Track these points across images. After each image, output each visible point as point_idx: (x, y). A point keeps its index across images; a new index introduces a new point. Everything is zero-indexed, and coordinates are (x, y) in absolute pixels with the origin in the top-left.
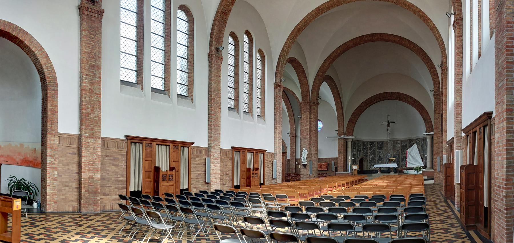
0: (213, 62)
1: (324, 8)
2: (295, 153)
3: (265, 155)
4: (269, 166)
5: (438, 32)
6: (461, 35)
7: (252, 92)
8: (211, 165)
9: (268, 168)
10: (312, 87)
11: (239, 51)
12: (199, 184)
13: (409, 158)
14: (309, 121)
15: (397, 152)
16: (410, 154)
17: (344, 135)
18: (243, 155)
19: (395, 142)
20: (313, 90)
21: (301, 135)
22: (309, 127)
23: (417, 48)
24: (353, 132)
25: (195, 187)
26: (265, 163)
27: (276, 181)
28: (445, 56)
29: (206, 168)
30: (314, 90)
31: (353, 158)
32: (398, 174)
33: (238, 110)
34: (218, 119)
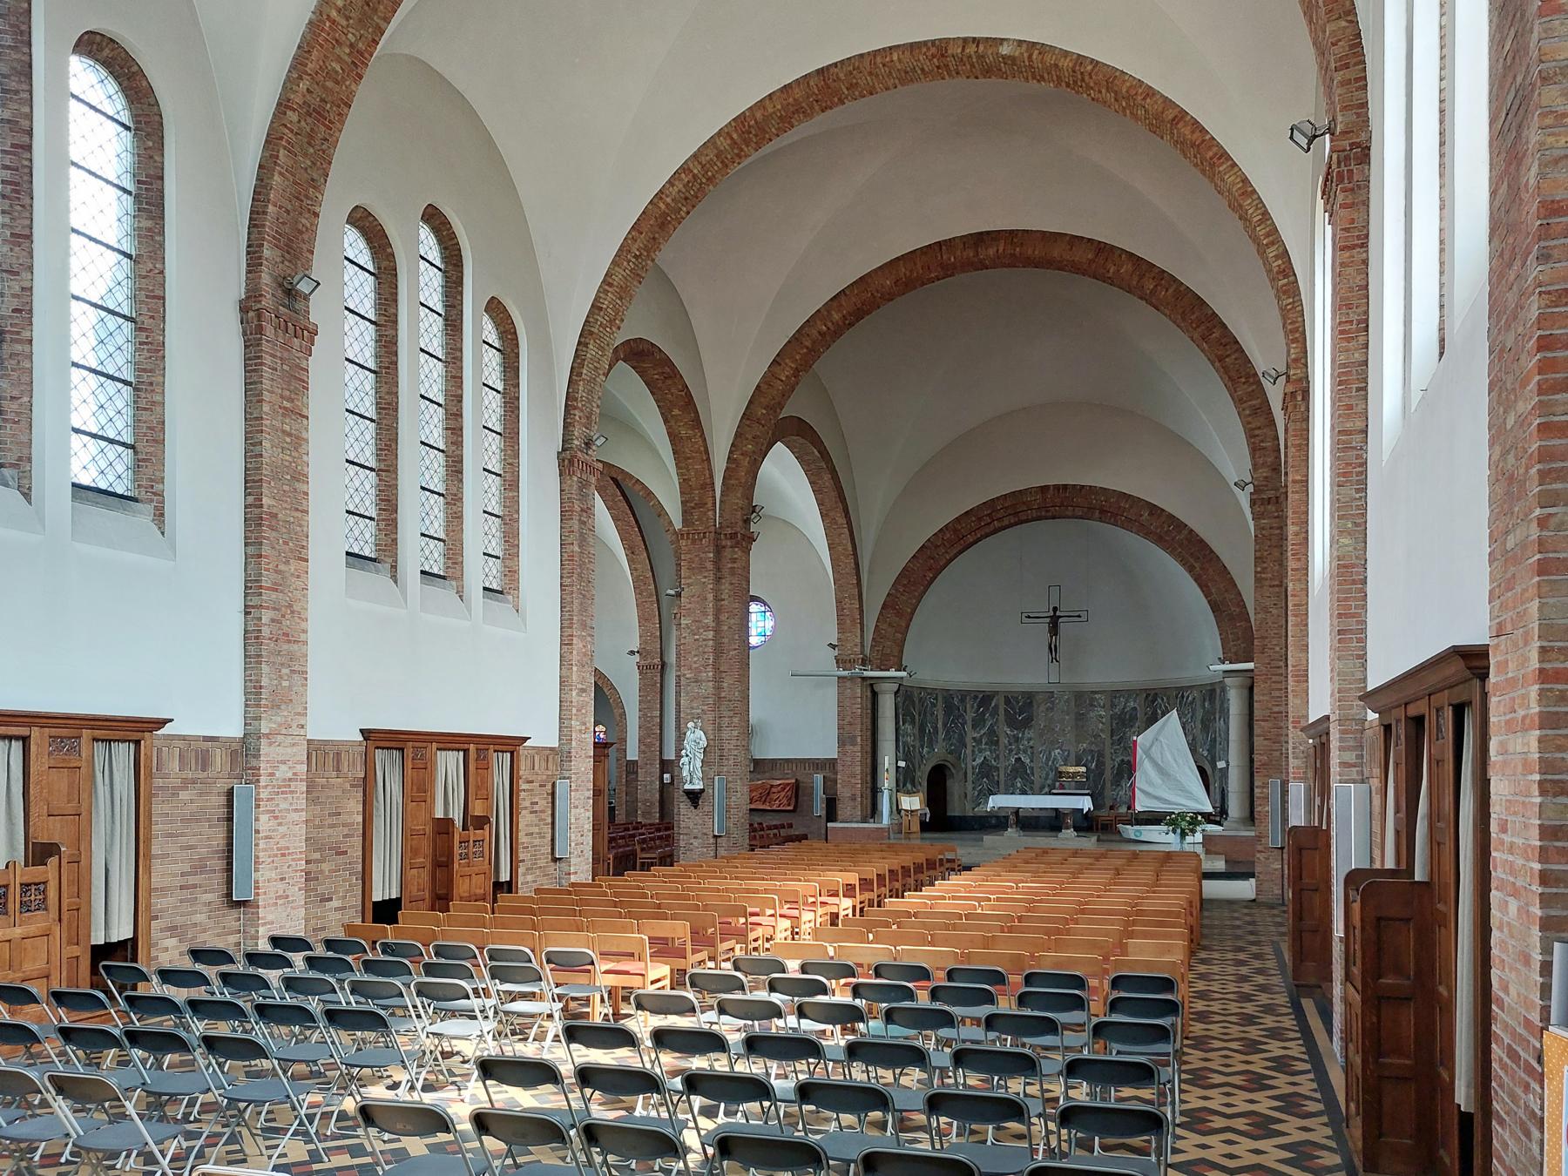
0: (265, 346)
1: (766, 118)
2: (661, 734)
3: (518, 760)
5: (1266, 213)
6: (1359, 237)
8: (257, 819)
9: (531, 813)
12: (195, 912)
14: (710, 611)
16: (1147, 753)
17: (863, 664)
18: (419, 764)
19: (1083, 699)
21: (679, 666)
22: (710, 637)
23: (1171, 291)
25: (172, 930)
26: (519, 791)
27: (566, 869)
28: (1296, 330)
29: (230, 831)
31: (902, 764)
32: (1094, 839)
33: (394, 567)
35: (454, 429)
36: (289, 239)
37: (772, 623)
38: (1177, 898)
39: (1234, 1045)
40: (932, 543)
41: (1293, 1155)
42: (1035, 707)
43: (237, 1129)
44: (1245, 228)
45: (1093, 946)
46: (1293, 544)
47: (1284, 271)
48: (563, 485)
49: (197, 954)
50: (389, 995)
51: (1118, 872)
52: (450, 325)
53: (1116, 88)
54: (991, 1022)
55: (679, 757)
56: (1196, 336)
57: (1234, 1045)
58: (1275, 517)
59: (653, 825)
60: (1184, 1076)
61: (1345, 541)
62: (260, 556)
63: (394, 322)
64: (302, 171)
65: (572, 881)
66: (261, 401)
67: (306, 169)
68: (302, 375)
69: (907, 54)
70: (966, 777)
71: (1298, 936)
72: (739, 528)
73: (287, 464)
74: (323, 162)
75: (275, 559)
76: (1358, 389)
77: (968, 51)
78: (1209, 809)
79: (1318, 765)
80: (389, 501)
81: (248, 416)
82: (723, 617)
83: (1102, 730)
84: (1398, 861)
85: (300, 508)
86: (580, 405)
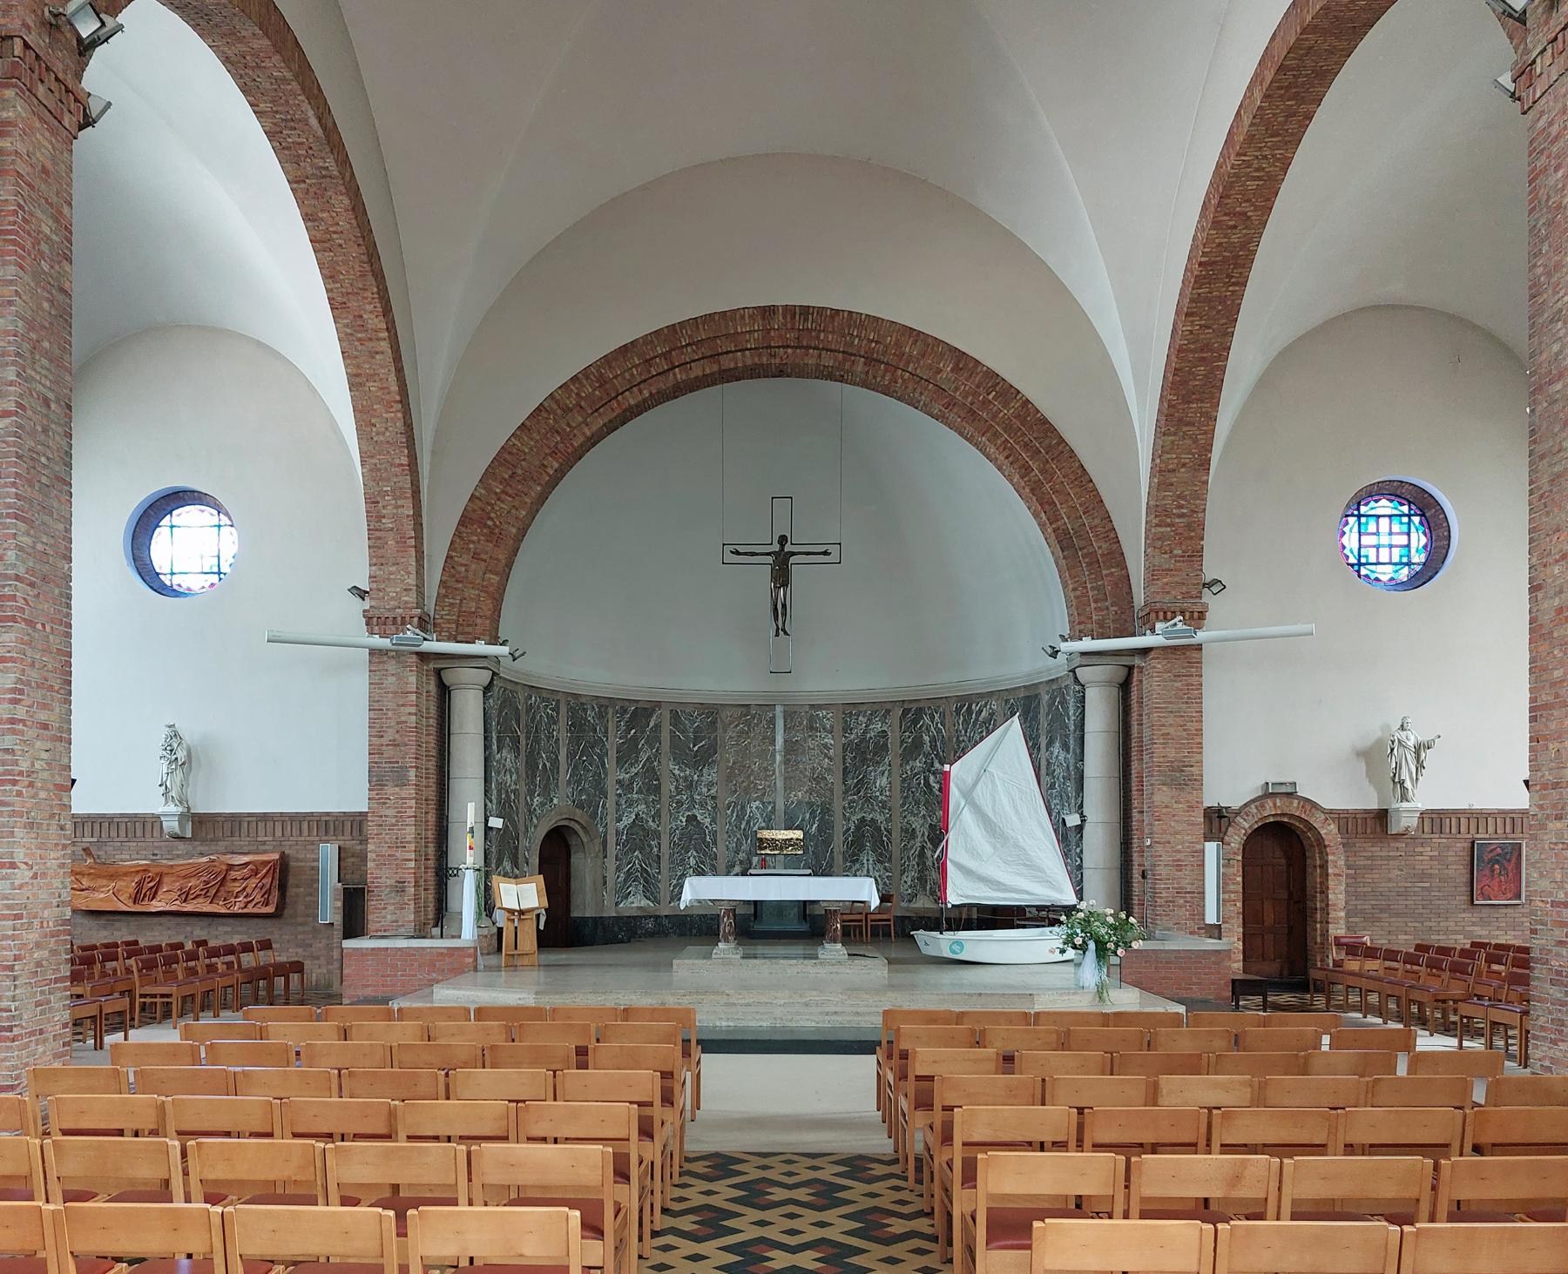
15: (810, 791)
16: (968, 795)
19: (804, 718)
24: (497, 611)
31: (497, 823)
40: (557, 402)
42: (720, 731)
50: (1444, 556)
83: (829, 770)
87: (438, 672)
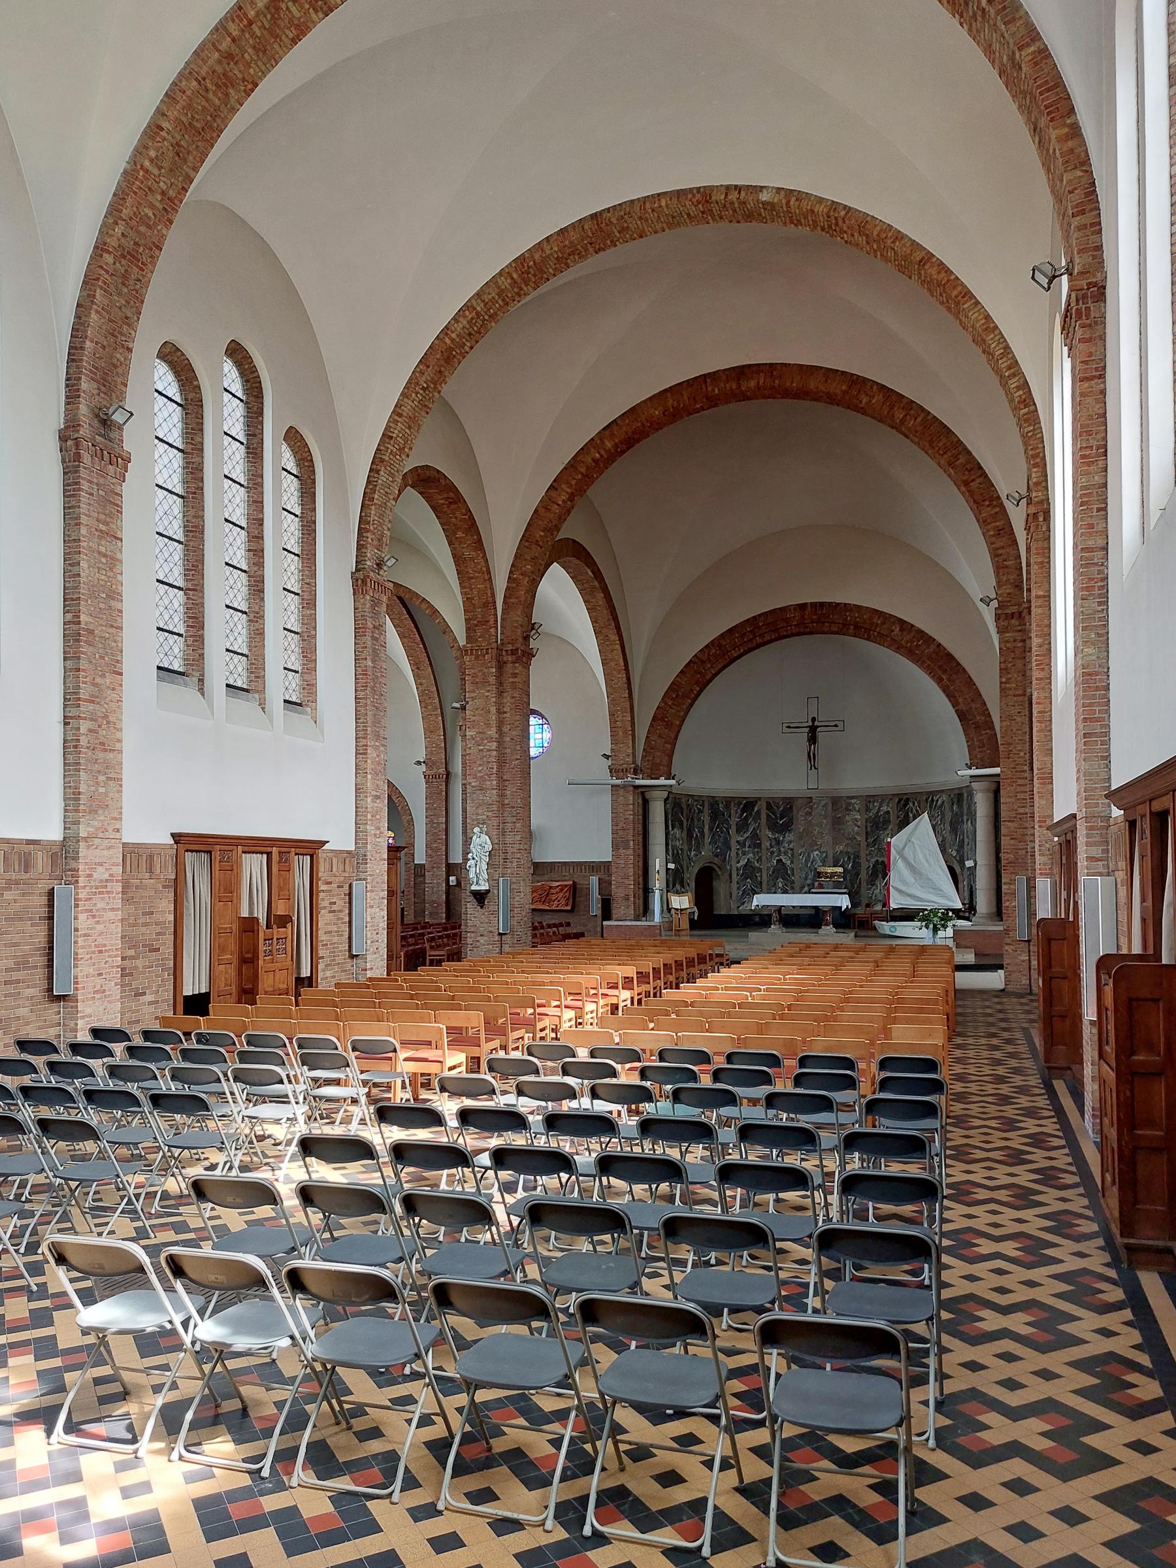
0: (83, 473)
1: (544, 259)
2: (447, 839)
3: (318, 863)
4: (335, 903)
5: (1007, 348)
6: (1096, 369)
7: (262, 607)
9: (330, 912)
10: (508, 588)
11: (202, 430)
12: (19, 1007)
13: (899, 872)
14: (494, 723)
16: (900, 853)
17: (635, 773)
19: (839, 804)
20: (508, 600)
21: (464, 775)
22: (494, 748)
23: (919, 419)
24: (670, 762)
27: (362, 965)
29: (51, 929)
30: (513, 600)
31: (671, 866)
33: (201, 680)
34: (111, 719)
35: (256, 551)
36: (104, 373)
37: (549, 735)
38: (934, 988)
39: (993, 1123)
40: (698, 658)
41: (1053, 1224)
42: (795, 811)
43: (68, 1208)
44: (989, 360)
45: (858, 1031)
46: (1037, 655)
47: (1025, 400)
48: (357, 604)
49: (23, 1045)
50: (205, 1081)
51: (877, 964)
52: (251, 453)
53: (867, 232)
54: (771, 1101)
55: (466, 860)
56: (942, 462)
57: (993, 1123)
58: (1020, 631)
59: (440, 924)
60: (948, 1152)
61: (1089, 650)
62: (78, 670)
63: (201, 450)
64: (117, 310)
65: (368, 976)
66: (78, 524)
67: (120, 308)
68: (117, 500)
69: (675, 200)
70: (731, 878)
71: (1049, 1020)
72: (519, 644)
73: (103, 583)
74: (136, 300)
75: (92, 672)
76: (1099, 510)
77: (730, 197)
78: (959, 905)
79: (1064, 861)
80: (196, 618)
81: (66, 539)
82: (506, 729)
83: (857, 833)
84: (1145, 946)
85: (115, 625)
86: (372, 528)
87: (643, 793)
